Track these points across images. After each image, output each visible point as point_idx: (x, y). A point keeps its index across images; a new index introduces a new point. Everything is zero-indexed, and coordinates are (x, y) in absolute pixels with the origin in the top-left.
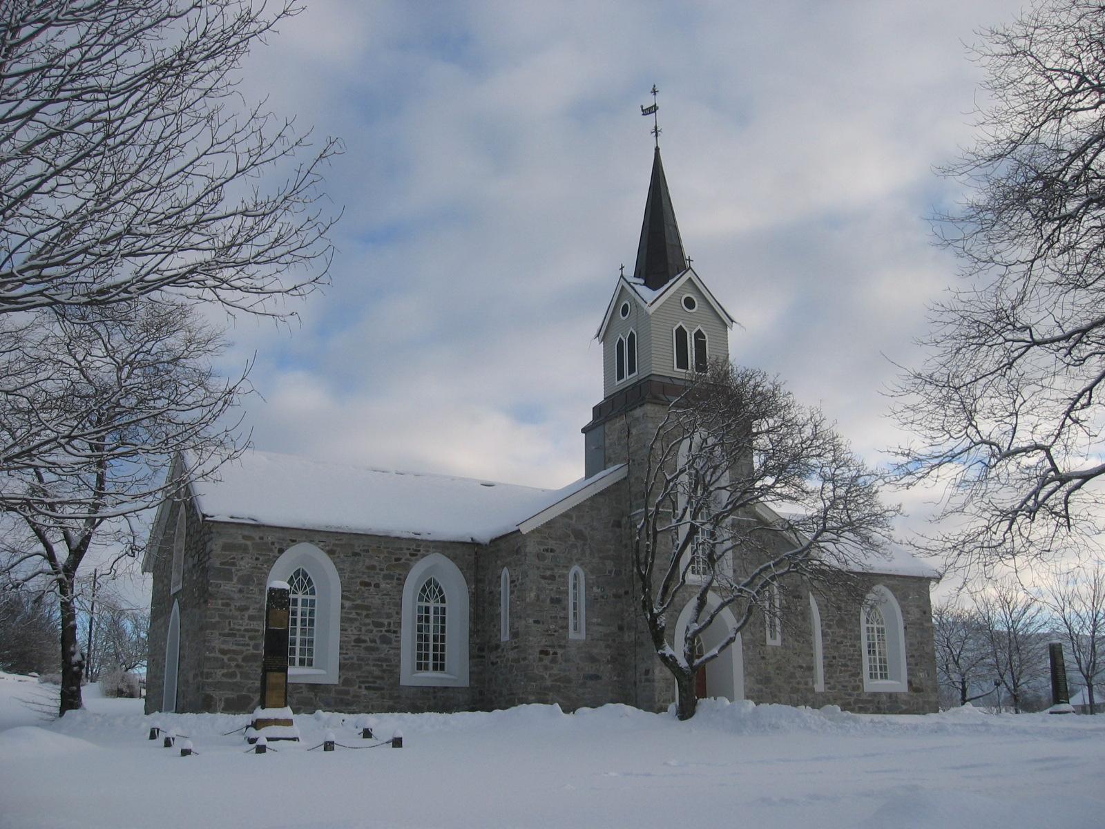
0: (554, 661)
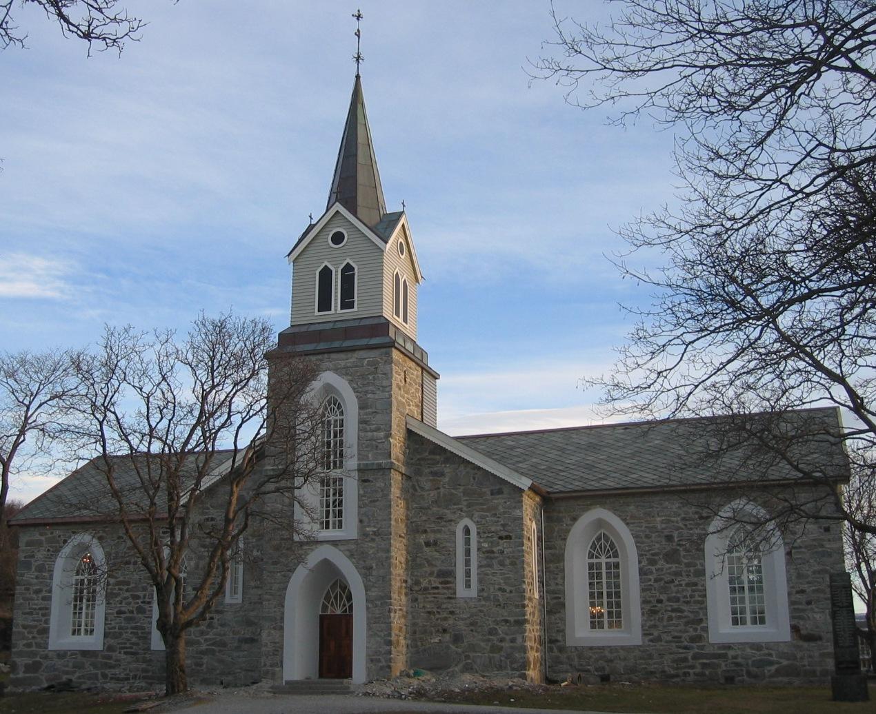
0: (210, 626)
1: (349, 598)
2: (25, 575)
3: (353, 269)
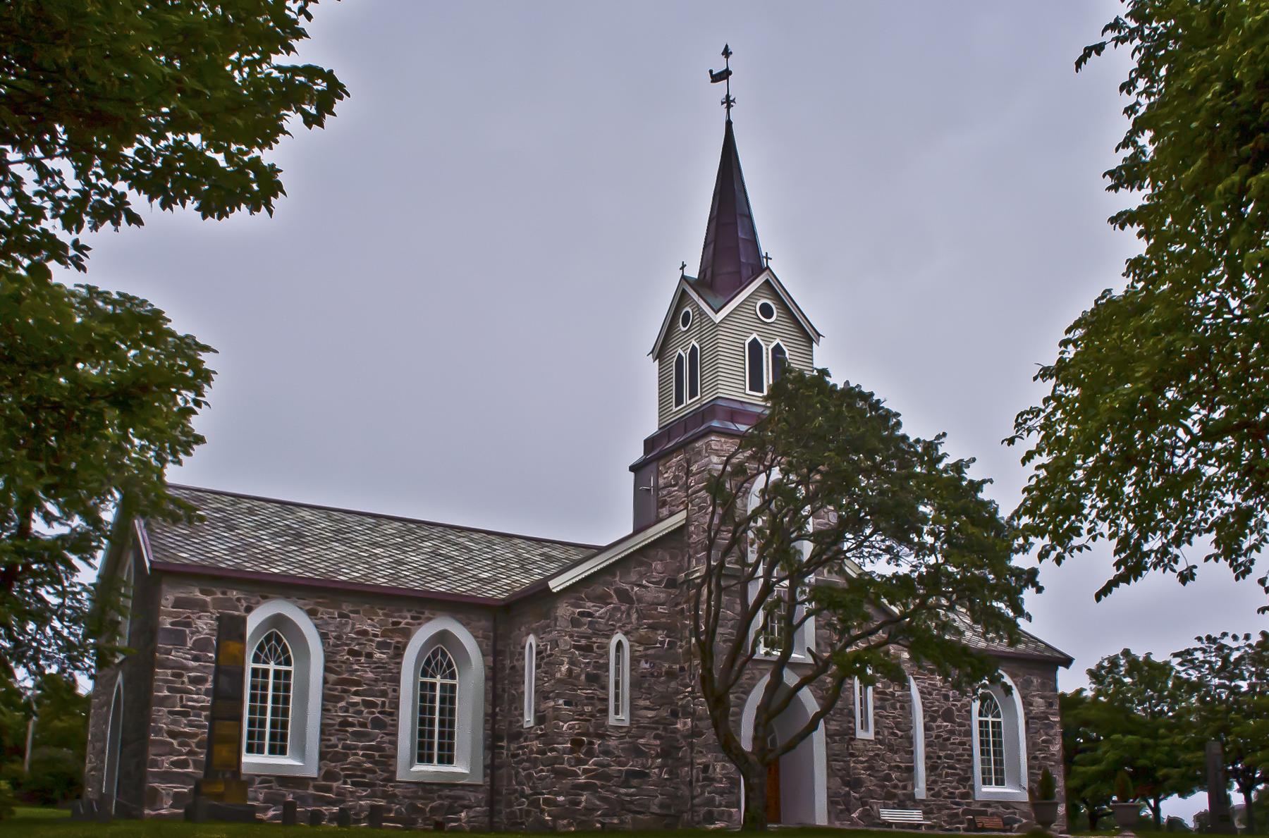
2: (173, 653)
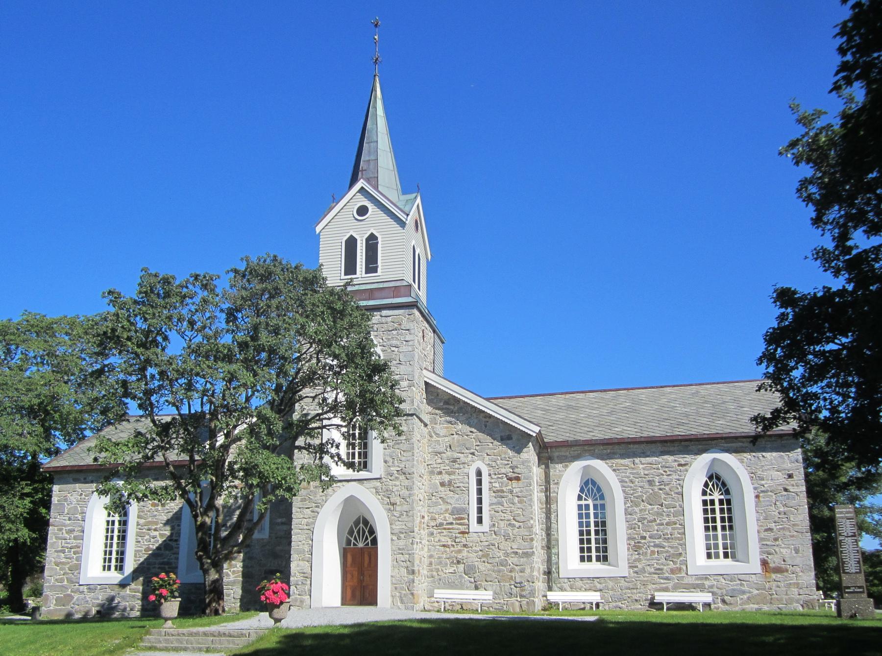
1: (372, 532)
3: (376, 238)
